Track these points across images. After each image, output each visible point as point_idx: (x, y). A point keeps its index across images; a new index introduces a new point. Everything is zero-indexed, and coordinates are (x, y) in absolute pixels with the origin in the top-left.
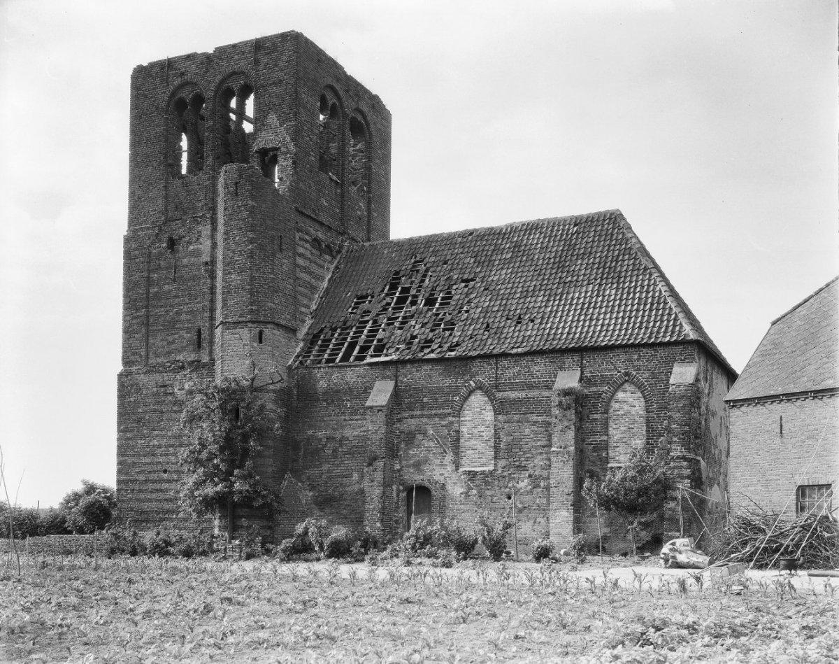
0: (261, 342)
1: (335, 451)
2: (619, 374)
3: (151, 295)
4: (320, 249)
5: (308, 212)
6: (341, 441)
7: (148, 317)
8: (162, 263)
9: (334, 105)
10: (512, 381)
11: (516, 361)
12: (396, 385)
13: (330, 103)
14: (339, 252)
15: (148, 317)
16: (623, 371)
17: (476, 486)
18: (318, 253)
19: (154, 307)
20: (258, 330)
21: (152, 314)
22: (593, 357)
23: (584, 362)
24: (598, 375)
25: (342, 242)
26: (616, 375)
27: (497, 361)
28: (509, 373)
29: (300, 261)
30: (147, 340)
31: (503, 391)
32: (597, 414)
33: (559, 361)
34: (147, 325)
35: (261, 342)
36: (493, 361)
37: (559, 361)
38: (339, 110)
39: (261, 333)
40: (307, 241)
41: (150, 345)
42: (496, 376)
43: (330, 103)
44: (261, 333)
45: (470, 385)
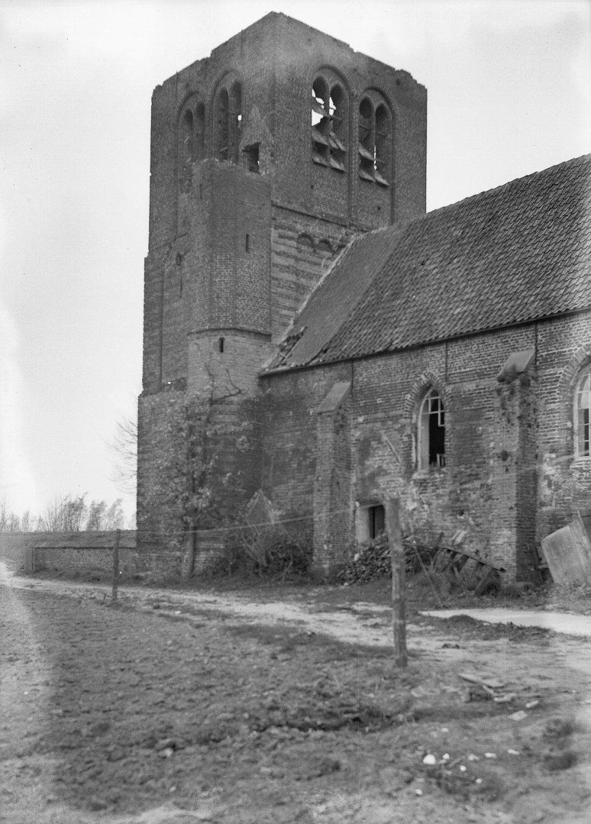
0: (222, 351)
1: (299, 464)
2: (579, 349)
3: (164, 314)
4: (312, 245)
5: (295, 206)
6: (304, 453)
7: (161, 336)
8: (172, 281)
9: (381, 108)
10: (462, 370)
11: (466, 346)
12: (352, 386)
13: (375, 106)
14: (341, 247)
15: (161, 336)
16: (584, 344)
17: (121, 605)
18: (311, 250)
19: (167, 326)
20: (219, 337)
21: (165, 333)
22: (550, 330)
23: (540, 337)
24: (555, 353)
25: (346, 234)
26: (575, 350)
27: (447, 347)
28: (459, 362)
29: (278, 260)
30: (161, 359)
31: (454, 383)
32: (555, 402)
33: (512, 340)
34: (161, 345)
35: (222, 351)
36: (442, 348)
37: (512, 340)
38: (346, 92)
39: (222, 341)
40: (291, 238)
41: (163, 365)
42: (446, 366)
43: (375, 106)
44: (222, 341)
45: (421, 379)
